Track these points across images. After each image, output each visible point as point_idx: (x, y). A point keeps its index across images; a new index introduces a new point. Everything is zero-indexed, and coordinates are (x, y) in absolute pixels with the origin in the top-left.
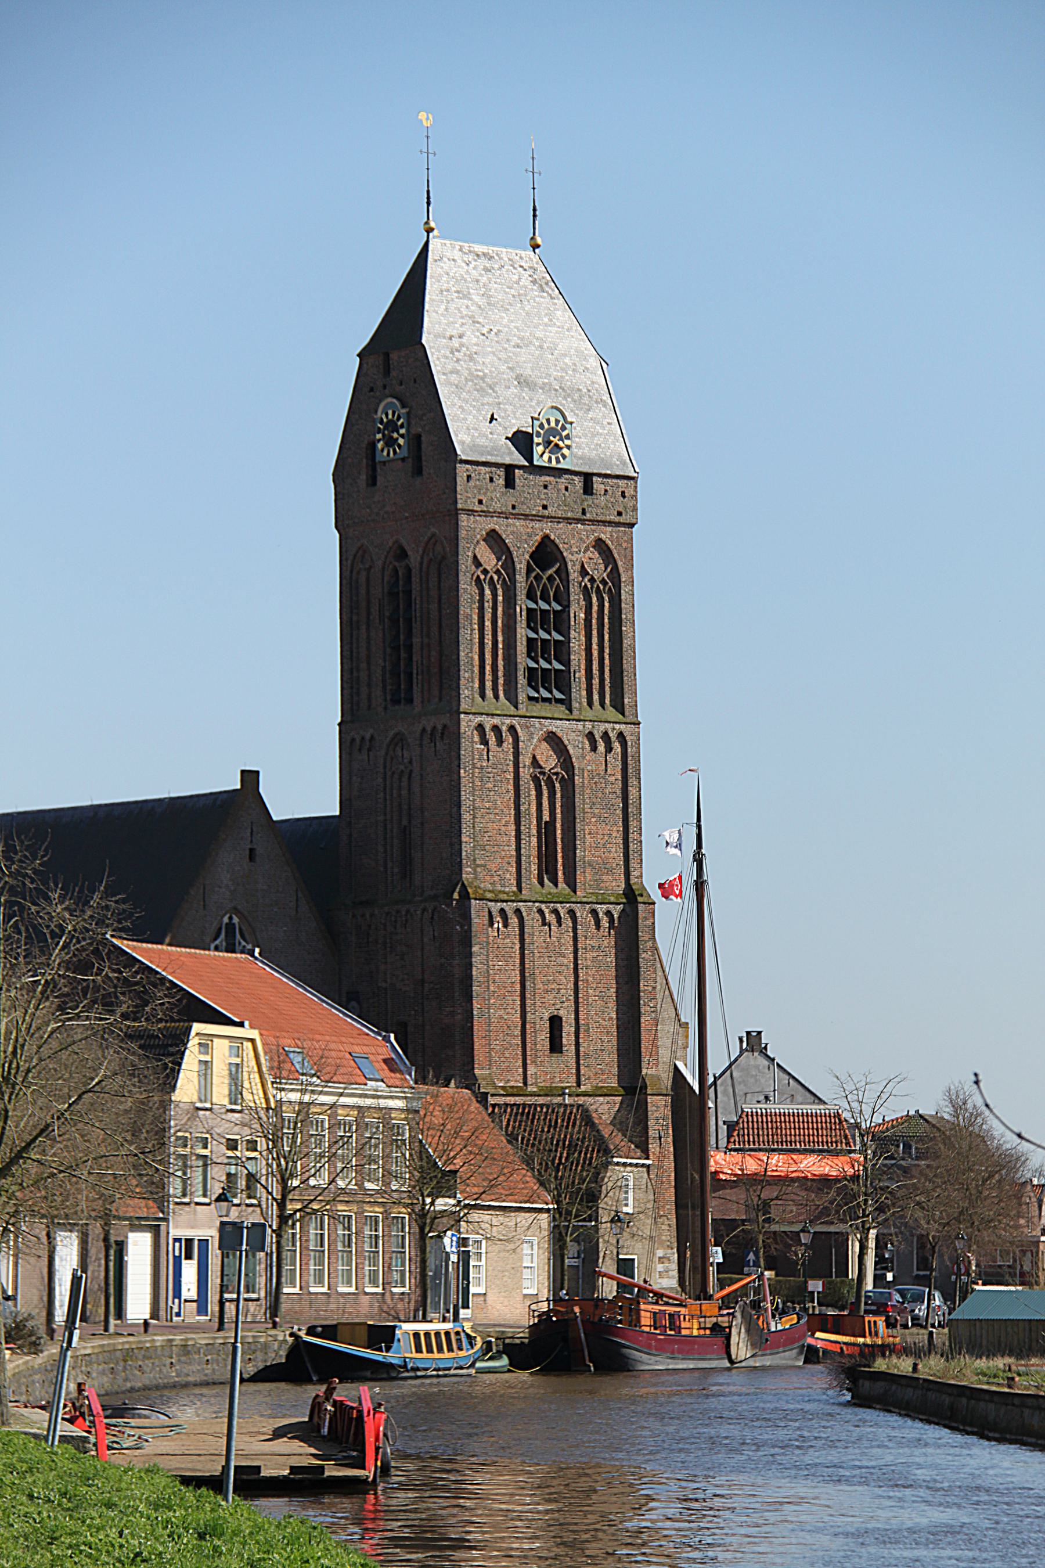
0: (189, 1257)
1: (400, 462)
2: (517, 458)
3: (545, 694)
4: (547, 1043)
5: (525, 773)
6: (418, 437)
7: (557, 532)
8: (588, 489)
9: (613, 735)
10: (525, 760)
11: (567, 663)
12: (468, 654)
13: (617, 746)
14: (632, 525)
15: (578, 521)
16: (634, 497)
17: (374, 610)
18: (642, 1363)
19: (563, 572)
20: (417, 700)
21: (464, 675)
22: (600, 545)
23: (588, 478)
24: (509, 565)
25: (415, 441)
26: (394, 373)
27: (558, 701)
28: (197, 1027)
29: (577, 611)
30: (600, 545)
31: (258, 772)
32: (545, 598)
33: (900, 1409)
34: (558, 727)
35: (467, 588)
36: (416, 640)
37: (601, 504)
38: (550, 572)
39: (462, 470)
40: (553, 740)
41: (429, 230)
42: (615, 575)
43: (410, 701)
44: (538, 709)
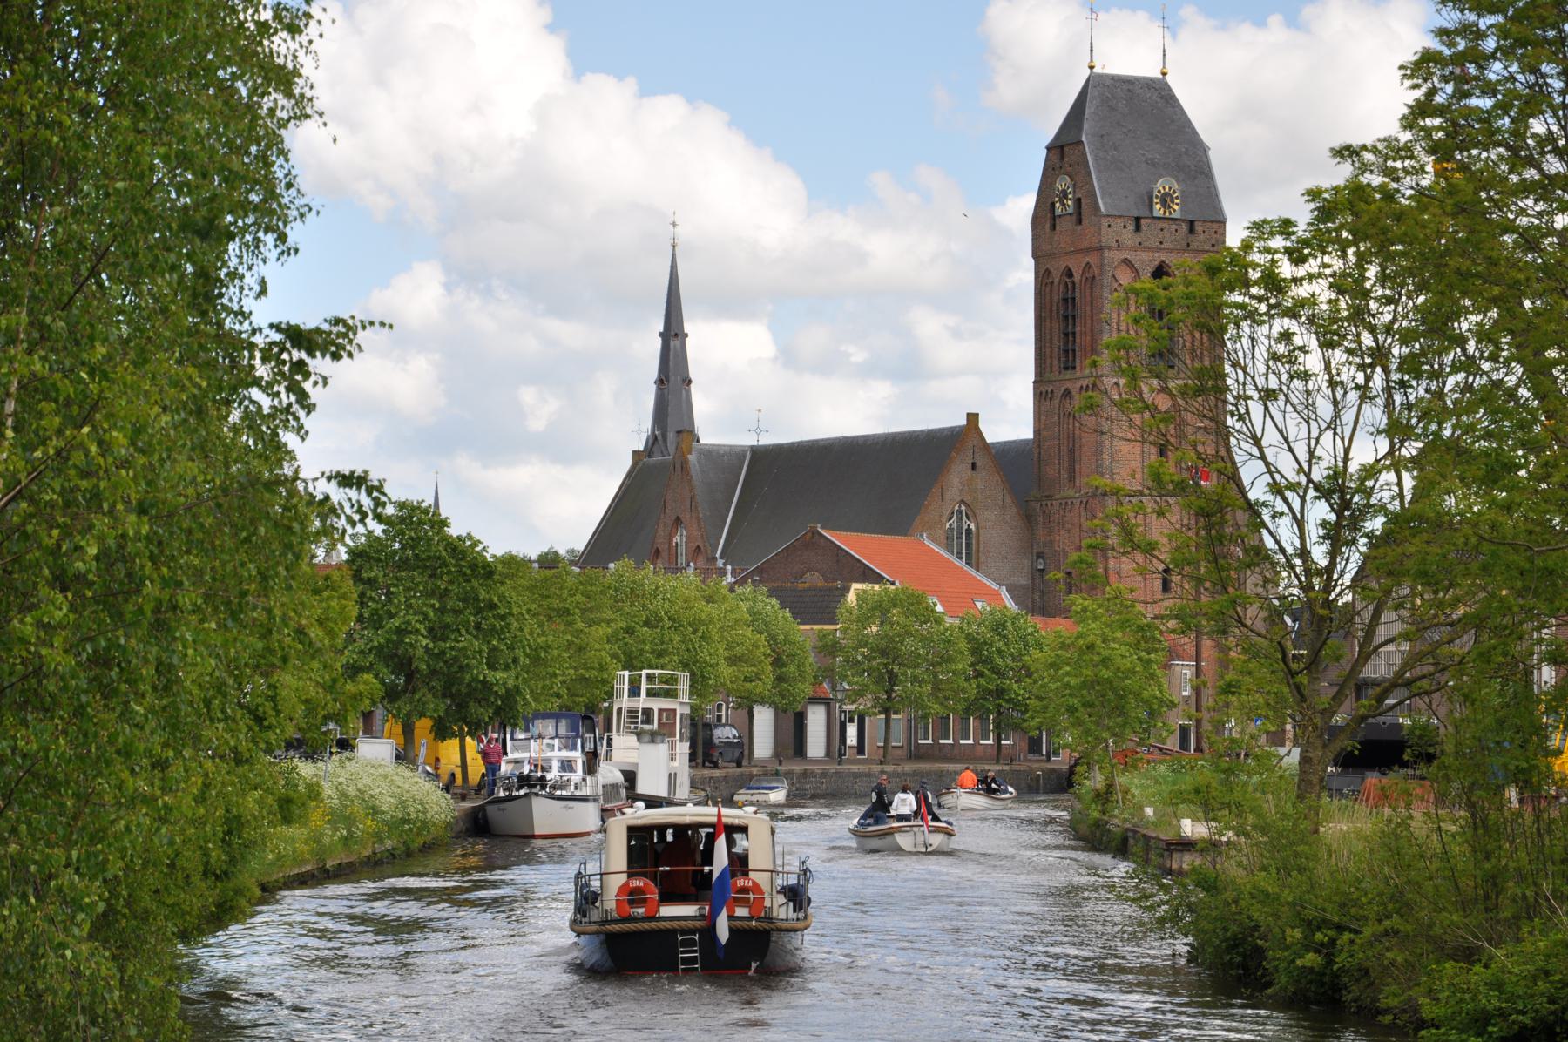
1: (1366, 408)
4: (1160, 587)
8: (1191, 230)
15: (1185, 251)
20: (1078, 368)
31: (968, 414)
43: (1074, 368)
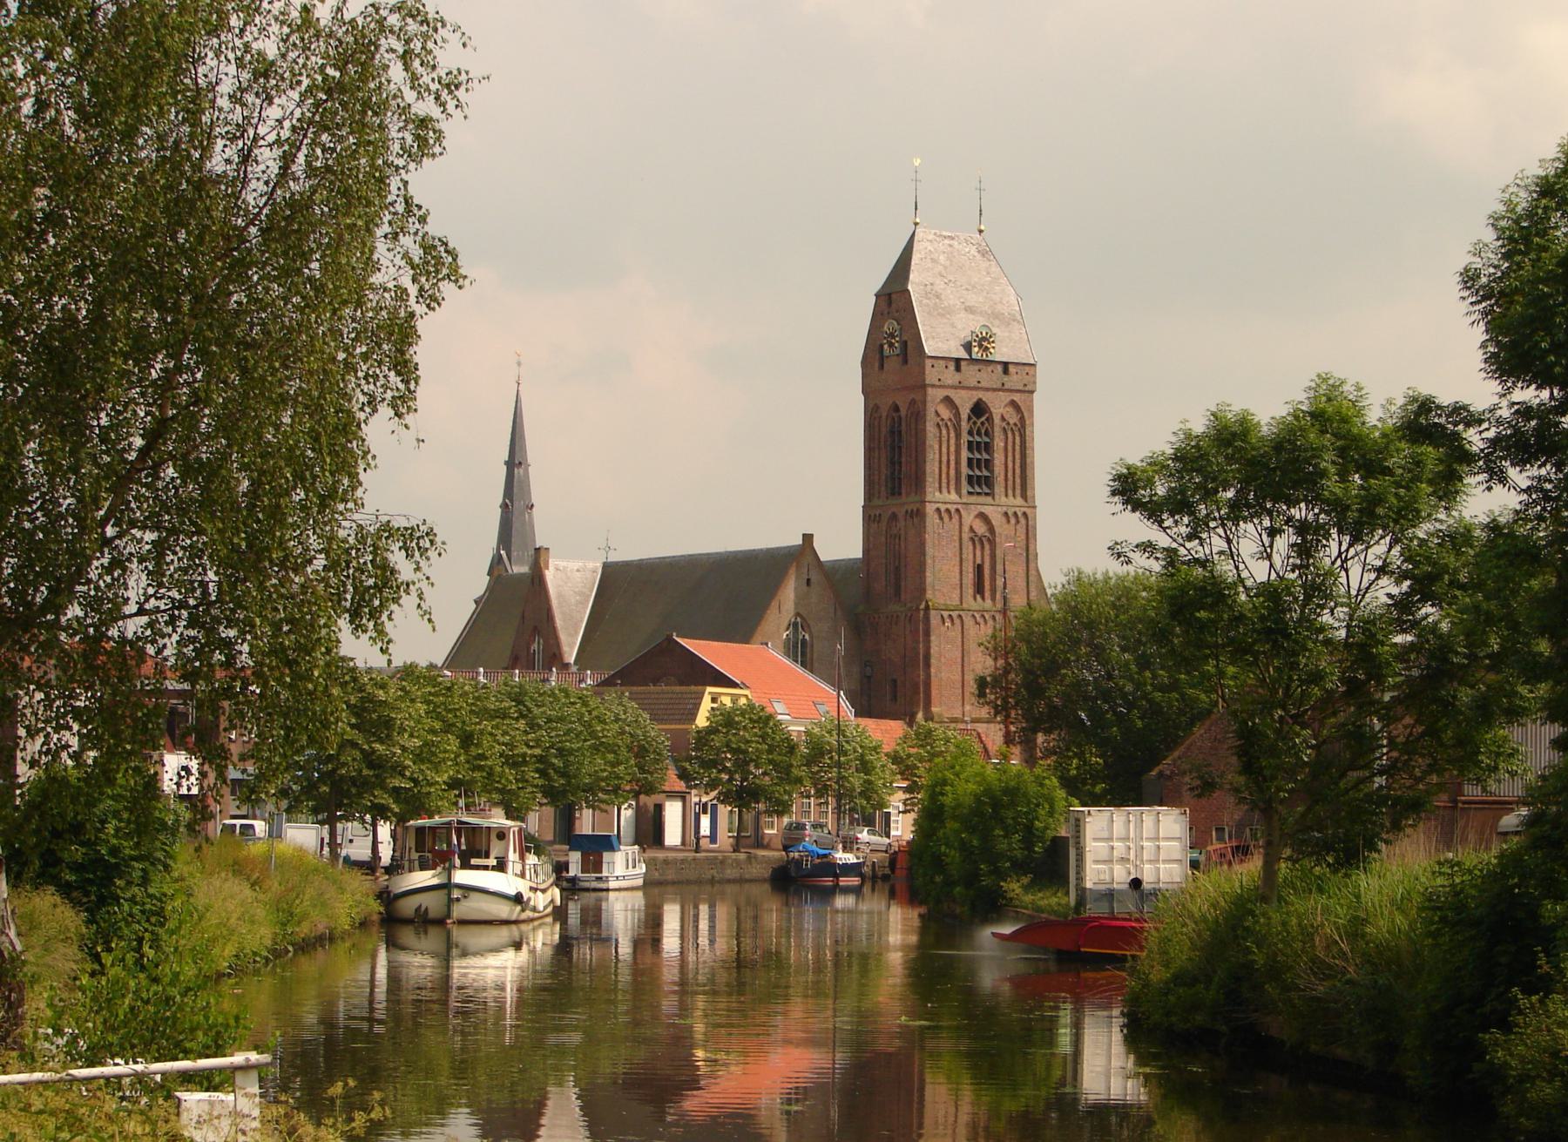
0: (705, 812)
2: (963, 354)
3: (979, 490)
5: (966, 536)
6: (906, 342)
7: (987, 397)
8: (1006, 371)
9: (1020, 514)
10: (966, 529)
11: (992, 472)
12: (932, 467)
13: (1023, 521)
14: (1032, 392)
15: (999, 390)
16: (1034, 376)
17: (882, 440)
18: (1464, 849)
19: (990, 419)
21: (929, 479)
22: (1013, 404)
23: (1006, 365)
24: (957, 414)
25: (904, 344)
26: (894, 305)
27: (987, 494)
28: (709, 689)
29: (999, 443)
30: (1013, 404)
32: (979, 434)
33: (1101, 926)
34: (987, 510)
35: (931, 429)
36: (903, 460)
37: (1014, 380)
38: (983, 419)
39: (928, 363)
40: (983, 517)
41: (916, 224)
42: (1022, 419)
43: (900, 494)
44: (973, 499)
